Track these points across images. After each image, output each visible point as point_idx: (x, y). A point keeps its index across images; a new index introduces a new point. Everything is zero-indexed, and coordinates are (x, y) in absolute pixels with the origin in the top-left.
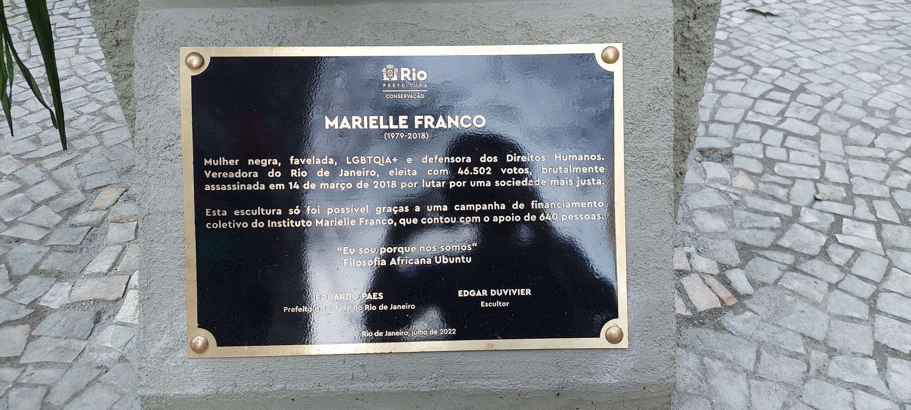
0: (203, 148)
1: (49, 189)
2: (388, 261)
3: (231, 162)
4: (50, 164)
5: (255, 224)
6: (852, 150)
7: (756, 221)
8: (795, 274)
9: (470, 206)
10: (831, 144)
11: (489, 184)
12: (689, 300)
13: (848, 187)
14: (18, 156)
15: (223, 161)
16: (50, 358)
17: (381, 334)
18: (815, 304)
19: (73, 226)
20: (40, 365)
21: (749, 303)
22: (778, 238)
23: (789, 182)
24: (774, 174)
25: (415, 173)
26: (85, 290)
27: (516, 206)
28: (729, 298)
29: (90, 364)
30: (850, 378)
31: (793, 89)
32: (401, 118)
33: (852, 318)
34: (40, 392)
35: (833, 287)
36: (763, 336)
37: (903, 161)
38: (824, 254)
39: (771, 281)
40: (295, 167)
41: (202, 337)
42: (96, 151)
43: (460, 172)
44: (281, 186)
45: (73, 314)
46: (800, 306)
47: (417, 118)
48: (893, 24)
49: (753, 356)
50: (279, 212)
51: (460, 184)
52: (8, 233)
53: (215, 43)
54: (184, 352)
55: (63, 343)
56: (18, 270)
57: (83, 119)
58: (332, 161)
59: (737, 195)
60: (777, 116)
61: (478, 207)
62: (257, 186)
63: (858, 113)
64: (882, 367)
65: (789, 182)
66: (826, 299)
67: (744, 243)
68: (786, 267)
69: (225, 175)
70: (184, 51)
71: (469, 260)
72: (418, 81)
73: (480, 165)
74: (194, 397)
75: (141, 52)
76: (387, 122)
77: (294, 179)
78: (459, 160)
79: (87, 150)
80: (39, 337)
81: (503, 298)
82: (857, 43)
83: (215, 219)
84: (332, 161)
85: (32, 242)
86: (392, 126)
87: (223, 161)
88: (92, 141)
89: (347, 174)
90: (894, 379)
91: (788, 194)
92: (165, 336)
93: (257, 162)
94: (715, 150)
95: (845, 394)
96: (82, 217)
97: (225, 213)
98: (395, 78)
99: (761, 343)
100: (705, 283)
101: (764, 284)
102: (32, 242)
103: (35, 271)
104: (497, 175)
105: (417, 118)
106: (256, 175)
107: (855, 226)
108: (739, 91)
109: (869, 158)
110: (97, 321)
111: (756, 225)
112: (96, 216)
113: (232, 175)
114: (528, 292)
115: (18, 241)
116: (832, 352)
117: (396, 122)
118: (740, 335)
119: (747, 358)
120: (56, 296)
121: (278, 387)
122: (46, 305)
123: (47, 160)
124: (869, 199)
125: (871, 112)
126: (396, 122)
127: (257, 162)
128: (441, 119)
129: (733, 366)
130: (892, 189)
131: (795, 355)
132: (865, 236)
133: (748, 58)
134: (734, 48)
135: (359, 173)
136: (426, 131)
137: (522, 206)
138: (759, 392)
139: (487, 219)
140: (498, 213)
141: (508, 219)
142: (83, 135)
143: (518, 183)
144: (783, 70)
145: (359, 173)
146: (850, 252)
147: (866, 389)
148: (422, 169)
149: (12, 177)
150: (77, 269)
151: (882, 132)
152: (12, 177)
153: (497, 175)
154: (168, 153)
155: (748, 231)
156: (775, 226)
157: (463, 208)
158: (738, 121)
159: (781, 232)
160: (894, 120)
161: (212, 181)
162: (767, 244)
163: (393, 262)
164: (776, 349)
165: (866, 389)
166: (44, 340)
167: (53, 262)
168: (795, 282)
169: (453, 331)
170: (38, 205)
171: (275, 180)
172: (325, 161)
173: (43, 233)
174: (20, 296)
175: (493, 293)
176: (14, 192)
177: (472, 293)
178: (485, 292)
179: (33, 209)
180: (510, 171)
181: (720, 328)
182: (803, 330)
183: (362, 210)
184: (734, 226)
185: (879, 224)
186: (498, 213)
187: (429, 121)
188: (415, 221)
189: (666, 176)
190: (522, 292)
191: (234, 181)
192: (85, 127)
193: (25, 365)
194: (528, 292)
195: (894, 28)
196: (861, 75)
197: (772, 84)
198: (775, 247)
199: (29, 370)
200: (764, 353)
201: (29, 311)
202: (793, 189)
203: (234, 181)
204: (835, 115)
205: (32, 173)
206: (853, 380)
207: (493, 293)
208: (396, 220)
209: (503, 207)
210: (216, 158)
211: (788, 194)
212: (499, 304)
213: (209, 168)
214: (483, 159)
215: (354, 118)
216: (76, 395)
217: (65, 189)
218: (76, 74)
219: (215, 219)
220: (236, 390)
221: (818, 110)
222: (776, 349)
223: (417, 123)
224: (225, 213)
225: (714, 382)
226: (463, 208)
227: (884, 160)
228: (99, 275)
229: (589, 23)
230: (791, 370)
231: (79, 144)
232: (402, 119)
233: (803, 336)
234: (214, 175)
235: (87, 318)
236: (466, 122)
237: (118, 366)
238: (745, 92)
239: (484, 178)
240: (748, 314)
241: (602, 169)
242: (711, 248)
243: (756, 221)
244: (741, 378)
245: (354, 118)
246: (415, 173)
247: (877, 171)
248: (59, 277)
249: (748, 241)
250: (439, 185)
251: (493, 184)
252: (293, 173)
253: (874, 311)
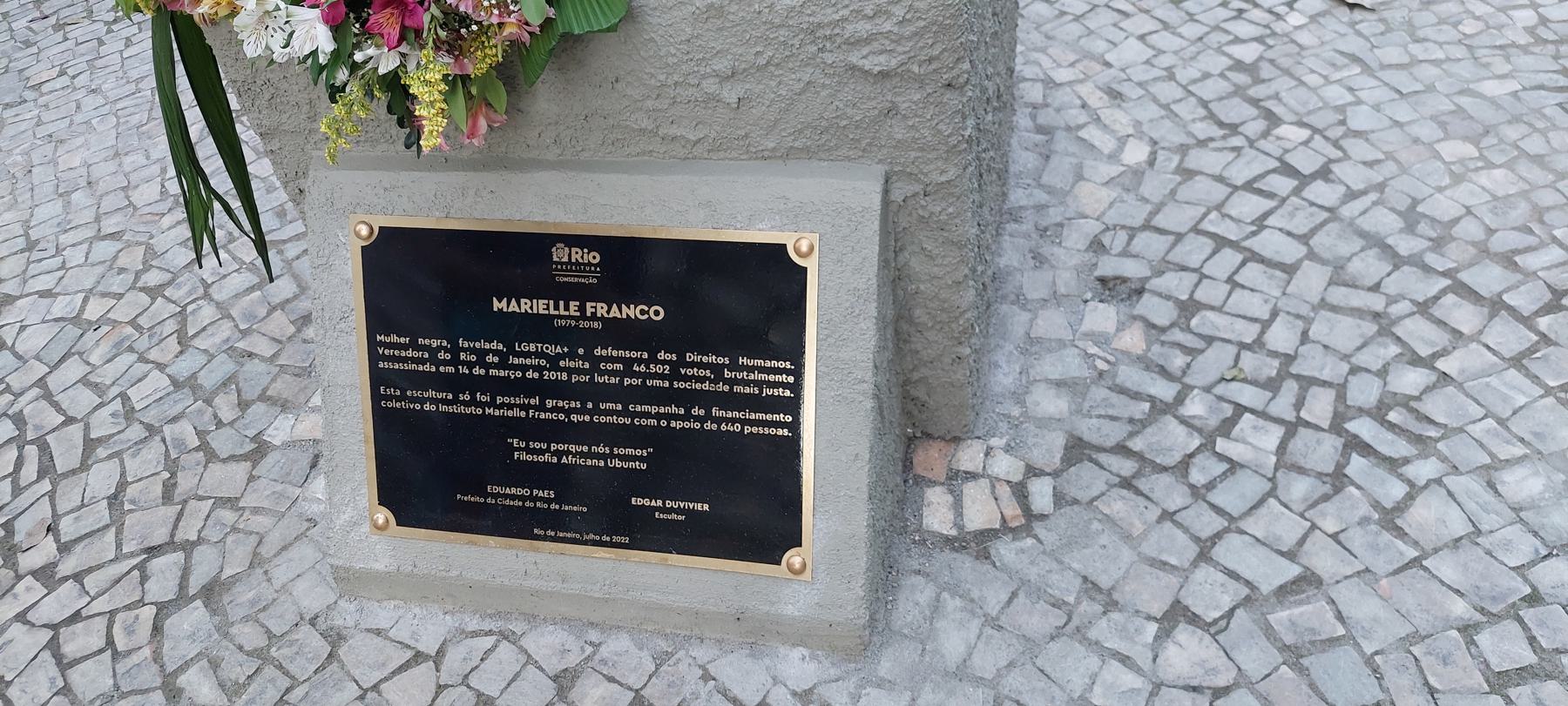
0: (378, 319)
3: (402, 340)
5: (427, 407)
7: (1113, 406)
8: (1124, 492)
9: (646, 408)
10: (1312, 280)
11: (667, 384)
12: (961, 515)
15: (394, 338)
16: (266, 504)
18: (1127, 537)
19: (305, 341)
20: (256, 511)
21: (1039, 529)
22: (1132, 435)
23: (1198, 344)
24: (1189, 330)
25: (587, 366)
27: (696, 411)
28: (1015, 517)
29: (300, 515)
30: (1112, 643)
31: (1306, 172)
32: (572, 304)
33: (1165, 563)
34: (253, 539)
35: (1167, 516)
36: (1033, 573)
37: (1407, 321)
40: (465, 350)
41: (383, 515)
43: (636, 368)
44: (451, 369)
47: (589, 305)
49: (1004, 597)
50: (450, 396)
51: (635, 381)
54: (366, 528)
55: (279, 487)
56: (247, 396)
58: (501, 347)
59: (1108, 362)
60: (1252, 223)
61: (654, 410)
62: (427, 367)
65: (1198, 344)
66: (1145, 534)
67: (1080, 439)
68: (1117, 480)
70: (354, 218)
71: (644, 467)
72: (590, 264)
73: (657, 362)
76: (557, 308)
78: (634, 354)
81: (679, 511)
82: (1484, 73)
83: (389, 398)
85: (263, 359)
86: (562, 312)
87: (394, 338)
91: (1188, 365)
93: (427, 342)
94: (1124, 280)
98: (565, 259)
99: (1024, 582)
100: (993, 492)
102: (263, 359)
103: (263, 397)
104: (675, 375)
105: (589, 305)
106: (426, 355)
107: (1255, 427)
108: (1217, 171)
111: (1110, 412)
113: (403, 354)
115: (250, 355)
116: (1111, 605)
117: (567, 308)
119: (994, 597)
120: (280, 430)
121: (454, 573)
123: (289, 245)
126: (567, 308)
127: (427, 342)
129: (973, 605)
131: (1057, 604)
132: (1261, 445)
133: (1269, 104)
134: (1258, 81)
135: (528, 361)
136: (598, 319)
137: (702, 412)
138: (987, 644)
139: (664, 423)
140: (676, 417)
141: (687, 425)
143: (698, 386)
144: (1315, 130)
145: (528, 361)
146: (1225, 466)
147: (1125, 660)
150: (302, 399)
151: (1405, 263)
153: (675, 375)
154: (343, 325)
155: (1094, 421)
156: (1137, 417)
157: (639, 408)
158: (1183, 230)
159: (1138, 426)
162: (1110, 443)
163: (564, 460)
167: (280, 388)
168: (1119, 505)
170: (274, 309)
171: (445, 363)
172: (494, 345)
173: (276, 347)
174: (246, 427)
175: (669, 504)
176: (252, 289)
177: (646, 502)
178: (660, 503)
179: (269, 314)
180: (690, 372)
181: (984, 555)
182: (1089, 572)
183: (532, 402)
184: (1079, 411)
186: (676, 417)
187: (602, 310)
189: (864, 393)
190: (699, 507)
191: (405, 360)
193: (243, 509)
197: (1280, 159)
198: (1122, 449)
199: (247, 513)
200: (1021, 595)
201: (254, 446)
202: (1200, 358)
203: (405, 360)
206: (1115, 646)
207: (669, 504)
209: (682, 411)
211: (1188, 365)
212: (674, 516)
213: (382, 344)
214: (662, 355)
216: (284, 548)
219: (389, 398)
221: (1325, 215)
222: (1038, 592)
223: (589, 312)
226: (639, 408)
229: (782, 207)
232: (573, 305)
233: (1085, 579)
236: (643, 312)
238: (1225, 174)
239: (662, 377)
240: (1030, 541)
242: (1031, 441)
243: (1113, 406)
244: (975, 624)
245: (523, 301)
246: (587, 366)
248: (284, 406)
249: (1086, 437)
251: (671, 384)
252: (463, 356)
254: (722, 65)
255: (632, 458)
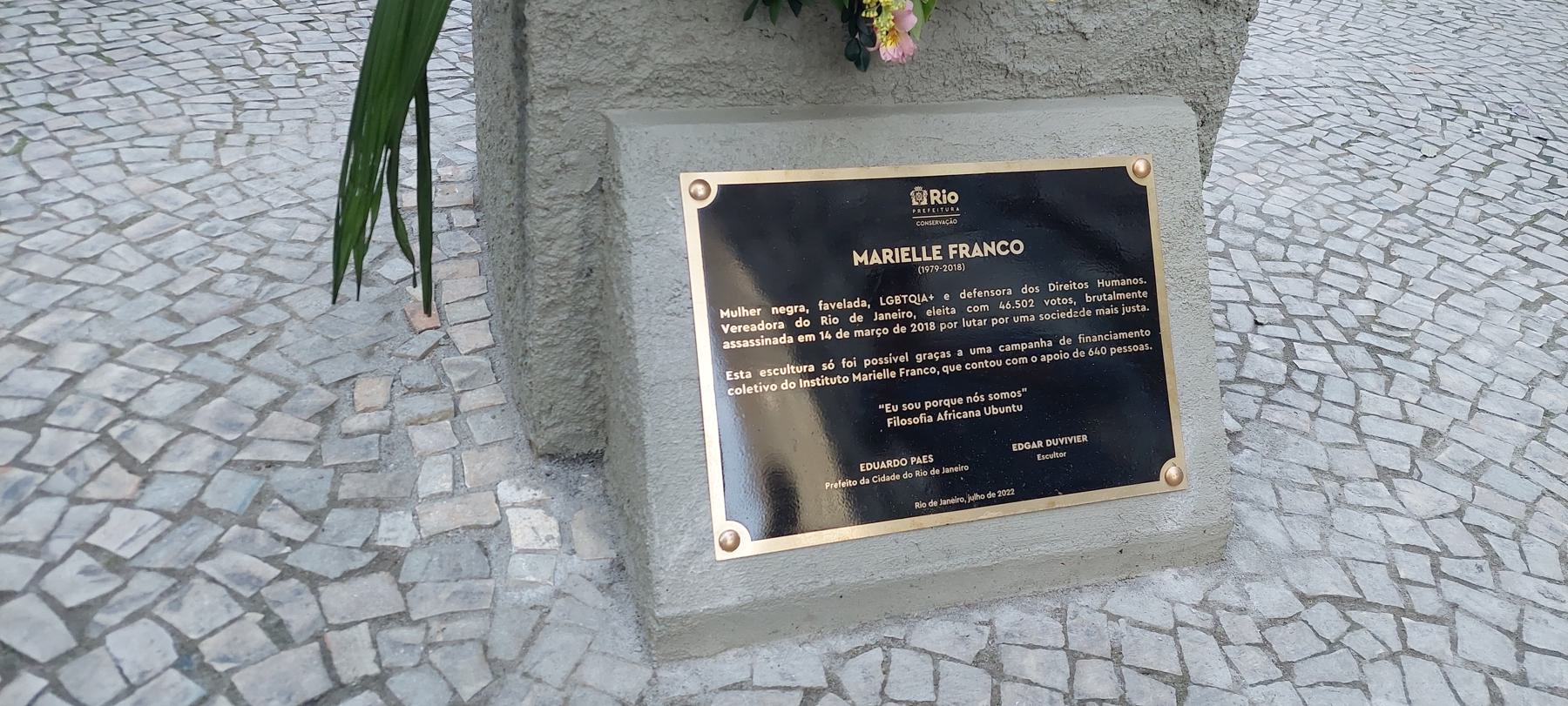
2: (935, 418)
3: (752, 312)
6: (1269, 266)
9: (1015, 346)
13: (1282, 307)
15: (742, 312)
17: (935, 504)
18: (1304, 434)
25: (954, 311)
32: (934, 248)
35: (1314, 415)
36: (1270, 472)
38: (1290, 382)
39: (1253, 417)
44: (811, 337)
46: (1292, 438)
47: (951, 247)
48: (1247, 111)
53: (721, 167)
58: (864, 304)
61: (1023, 347)
63: (1257, 223)
64: (1392, 489)
69: (746, 328)
70: (686, 179)
74: (726, 610)
77: (825, 328)
80: (414, 584)
81: (1059, 448)
84: (864, 304)
86: (926, 259)
87: (742, 312)
89: (882, 317)
90: (1406, 498)
92: (686, 537)
95: (1369, 518)
97: (749, 375)
98: (925, 202)
101: (1248, 420)
104: (1040, 308)
105: (951, 247)
109: (1288, 274)
113: (754, 328)
114: (1085, 438)
117: (929, 254)
118: (1250, 474)
121: (827, 582)
122: (388, 544)
124: (1309, 319)
125: (1269, 220)
128: (976, 246)
130: (1327, 307)
131: (1310, 488)
135: (894, 316)
139: (1034, 359)
140: (1045, 351)
141: (1057, 357)
145: (894, 316)
147: (1386, 510)
148: (961, 305)
153: (1040, 308)
157: (1008, 348)
160: (1296, 229)
161: (731, 337)
164: (1292, 485)
165: (1386, 510)
166: (425, 588)
168: (1277, 415)
171: (804, 331)
172: (858, 303)
175: (1049, 443)
177: (1027, 446)
180: (1053, 302)
183: (902, 358)
185: (1329, 345)
186: (1045, 351)
188: (959, 368)
194: (1085, 438)
195: (1249, 116)
196: (1242, 176)
204: (1234, 226)
207: (1049, 443)
208: (939, 369)
210: (734, 309)
212: (1055, 455)
214: (1025, 290)
215: (884, 251)
218: (155, 209)
220: (777, 594)
222: (1292, 485)
223: (952, 253)
224: (749, 375)
225: (1248, 523)
227: (1305, 275)
229: (1117, 133)
230: (1314, 503)
232: (935, 249)
234: (734, 329)
237: (560, 602)
239: (1027, 312)
241: (1145, 294)
244: (1271, 515)
245: (884, 251)
246: (954, 311)
247: (1303, 288)
250: (980, 323)
251: (1037, 318)
252: (824, 320)
253: (1360, 434)
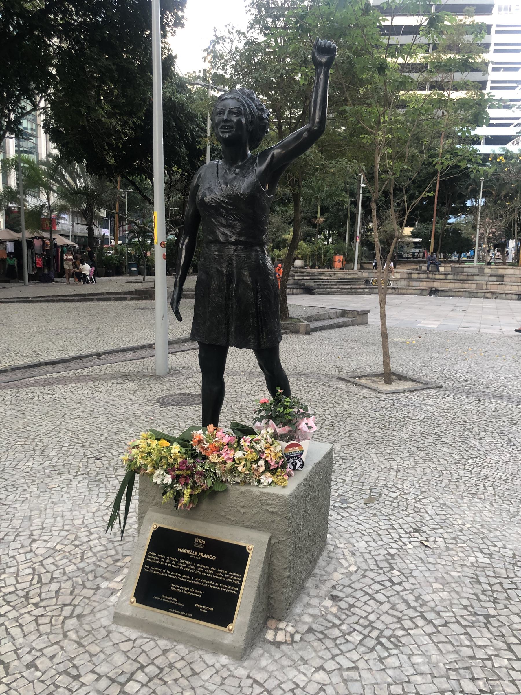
1: (113, 552)
4: (116, 544)
14: (108, 539)
15: (153, 553)
20: (94, 601)
21: (294, 645)
26: (112, 585)
34: (92, 608)
41: (134, 599)
42: (131, 543)
45: (106, 590)
51: (205, 574)
52: (98, 563)
54: (128, 603)
56: (97, 575)
57: (131, 530)
75: (145, 521)
79: (128, 542)
81: (206, 610)
87: (153, 553)
88: (131, 539)
96: (119, 564)
103: (101, 576)
108: (372, 577)
110: (112, 594)
112: (123, 564)
115: (100, 566)
140: (212, 585)
142: (129, 536)
149: (104, 546)
152: (104, 546)
161: (149, 558)
167: (107, 575)
169: (191, 615)
177: (199, 606)
186: (212, 585)
192: (131, 533)
205: (110, 546)
217: (117, 553)
228: (117, 582)
231: (127, 539)
235: (110, 592)
239: (211, 574)
248: (107, 579)
254: (242, 504)
255: (198, 594)
